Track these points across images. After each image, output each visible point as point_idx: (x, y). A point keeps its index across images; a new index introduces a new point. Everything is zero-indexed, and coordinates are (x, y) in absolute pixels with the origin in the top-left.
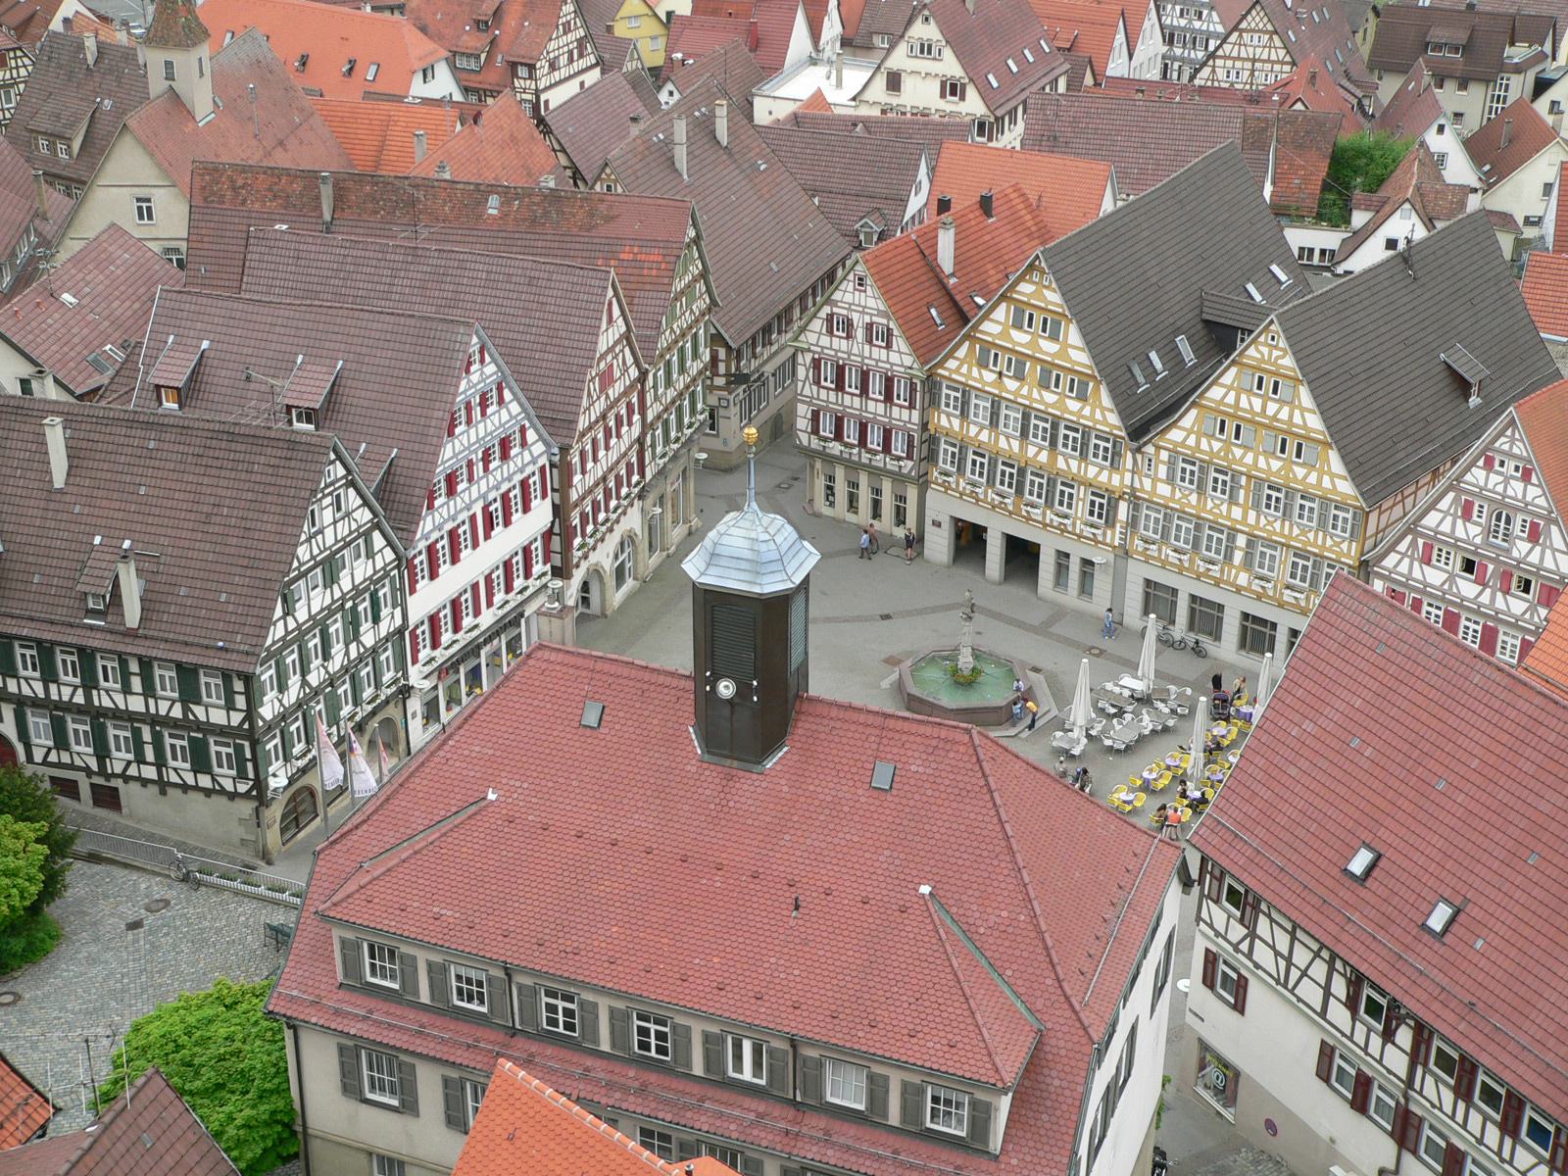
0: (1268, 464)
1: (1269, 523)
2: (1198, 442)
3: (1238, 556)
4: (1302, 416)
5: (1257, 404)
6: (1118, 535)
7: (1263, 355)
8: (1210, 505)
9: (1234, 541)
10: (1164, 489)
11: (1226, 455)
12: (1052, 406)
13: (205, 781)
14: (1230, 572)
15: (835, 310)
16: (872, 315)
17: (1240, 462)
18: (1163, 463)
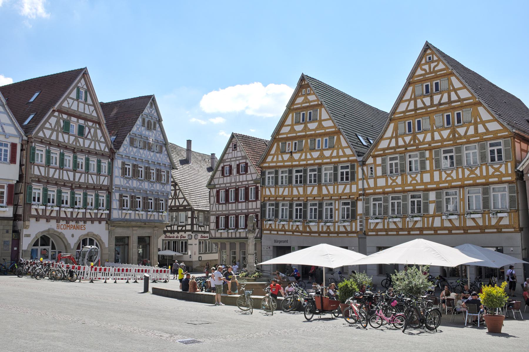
0: (441, 136)
1: (414, 179)
2: (397, 142)
3: (432, 208)
4: (456, 94)
5: (427, 101)
6: (359, 224)
7: (425, 70)
8: (409, 179)
9: (427, 199)
10: (381, 182)
11: (415, 141)
12: (318, 158)
13: (81, 122)
14: (428, 221)
15: (225, 164)
16: (239, 160)
17: (423, 143)
18: (379, 165)
